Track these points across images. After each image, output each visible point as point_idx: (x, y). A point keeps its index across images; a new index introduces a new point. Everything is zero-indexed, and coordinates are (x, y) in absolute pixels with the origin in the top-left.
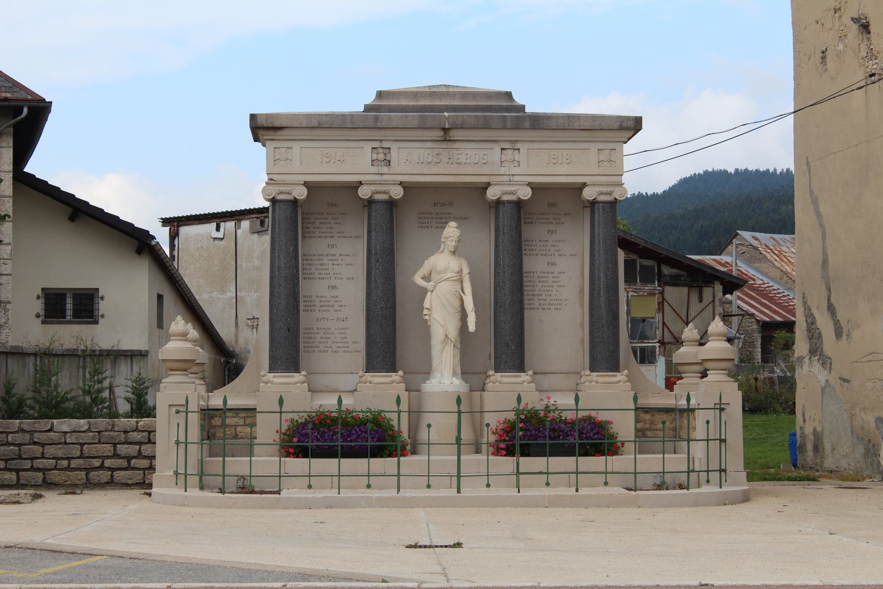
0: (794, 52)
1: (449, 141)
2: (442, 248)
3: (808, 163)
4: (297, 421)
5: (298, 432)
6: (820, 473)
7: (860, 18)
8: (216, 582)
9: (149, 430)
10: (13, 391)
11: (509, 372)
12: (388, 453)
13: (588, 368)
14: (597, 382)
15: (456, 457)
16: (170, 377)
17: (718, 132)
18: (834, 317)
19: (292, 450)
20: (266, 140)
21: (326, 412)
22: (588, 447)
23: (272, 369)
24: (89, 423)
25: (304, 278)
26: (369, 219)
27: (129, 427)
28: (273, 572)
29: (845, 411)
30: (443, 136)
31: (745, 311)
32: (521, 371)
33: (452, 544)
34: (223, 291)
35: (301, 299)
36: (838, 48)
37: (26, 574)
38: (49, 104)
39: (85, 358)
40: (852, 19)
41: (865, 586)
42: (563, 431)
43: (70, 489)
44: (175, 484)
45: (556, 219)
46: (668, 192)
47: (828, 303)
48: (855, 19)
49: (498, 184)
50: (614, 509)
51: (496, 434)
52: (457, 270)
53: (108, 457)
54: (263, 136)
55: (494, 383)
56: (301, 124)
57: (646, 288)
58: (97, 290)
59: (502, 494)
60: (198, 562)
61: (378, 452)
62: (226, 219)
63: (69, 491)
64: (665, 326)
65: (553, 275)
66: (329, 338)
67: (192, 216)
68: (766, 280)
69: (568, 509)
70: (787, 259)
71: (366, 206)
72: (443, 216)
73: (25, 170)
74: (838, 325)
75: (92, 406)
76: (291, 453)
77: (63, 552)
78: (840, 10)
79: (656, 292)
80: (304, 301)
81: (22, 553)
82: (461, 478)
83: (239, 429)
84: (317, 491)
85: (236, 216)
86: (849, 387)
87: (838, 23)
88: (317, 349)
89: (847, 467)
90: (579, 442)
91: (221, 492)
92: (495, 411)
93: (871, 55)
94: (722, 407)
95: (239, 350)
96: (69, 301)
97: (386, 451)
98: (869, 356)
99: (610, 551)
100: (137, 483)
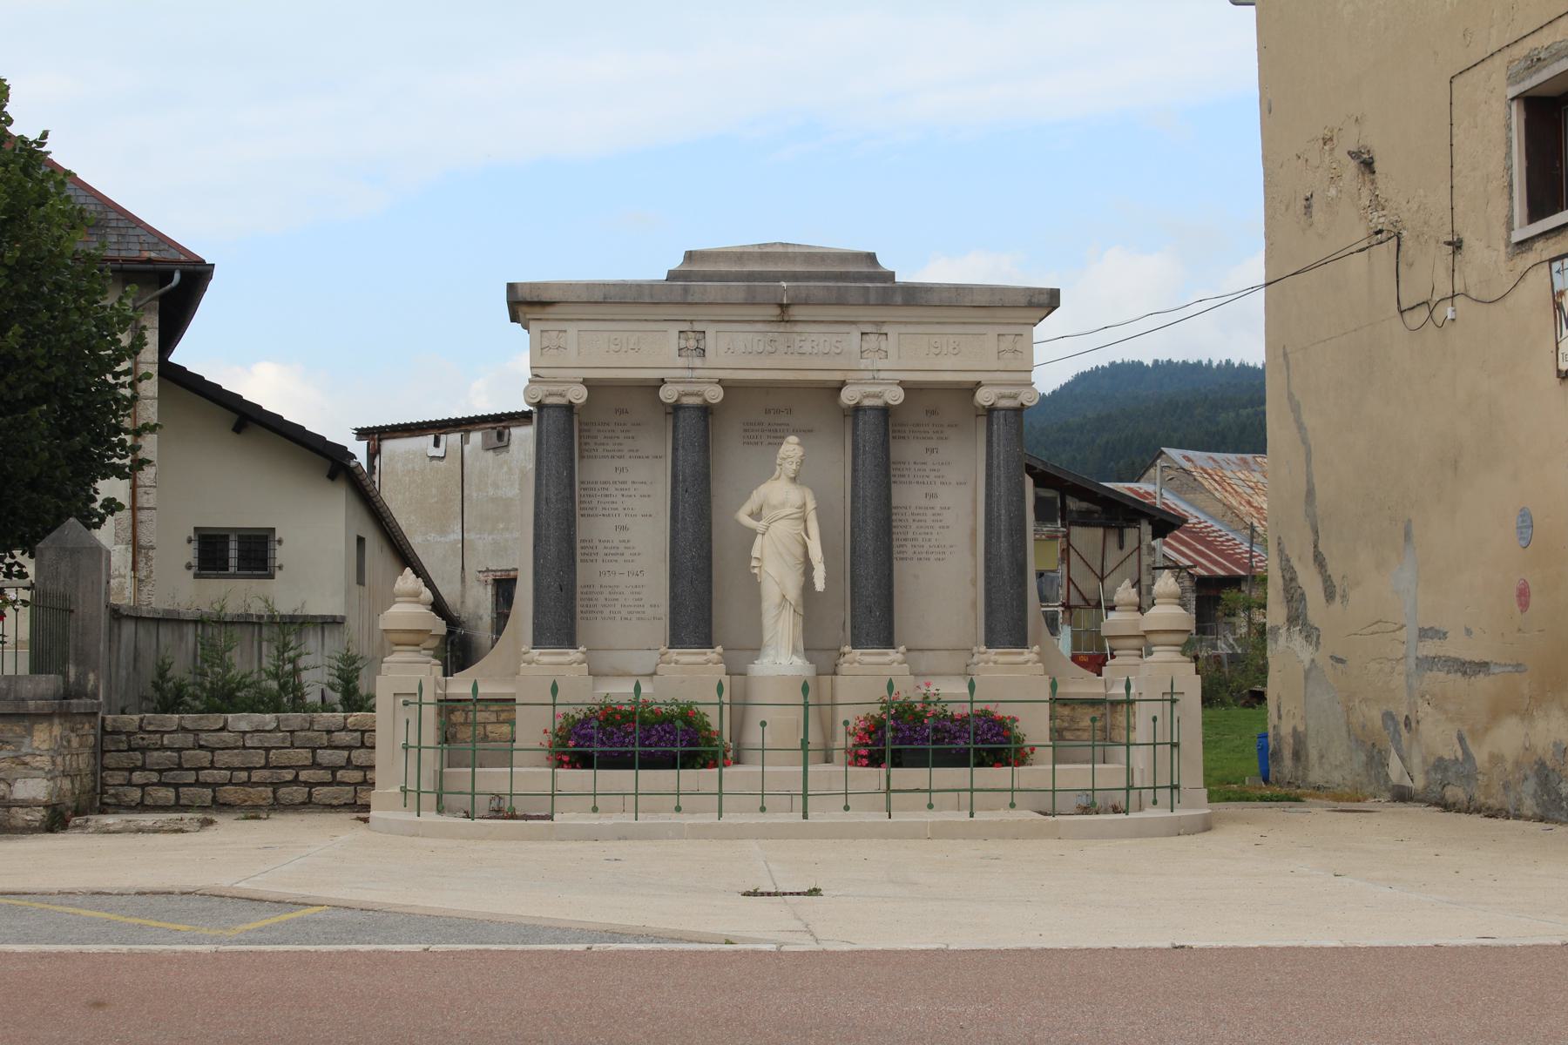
0: (1266, 198)
1: (787, 321)
2: (777, 473)
3: (1285, 355)
4: (573, 716)
7: (1360, 152)
8: (491, 944)
9: (363, 729)
10: (169, 674)
11: (872, 648)
13: (983, 642)
14: (995, 663)
15: (801, 769)
17: (1173, 308)
18: (1323, 570)
19: (565, 758)
21: (614, 704)
22: (985, 754)
23: (537, 643)
24: (278, 718)
25: (582, 515)
26: (674, 432)
28: (568, 929)
30: (780, 315)
31: (1173, 561)
34: (443, 531)
36: (1329, 194)
37: (220, 931)
38: (210, 267)
40: (1349, 153)
41: (1402, 947)
42: (949, 732)
45: (937, 432)
47: (1315, 552)
48: (1354, 153)
49: (858, 383)
52: (799, 503)
53: (305, 767)
54: (525, 314)
56: (579, 297)
57: (1045, 529)
58: (273, 530)
59: (867, 821)
61: (691, 760)
62: (448, 429)
64: (1071, 583)
65: (934, 511)
66: (617, 600)
67: (399, 425)
70: (1233, 489)
72: (778, 428)
73: (170, 359)
75: (280, 695)
76: (565, 762)
78: (1332, 140)
79: (1059, 534)
80: (582, 548)
83: (489, 728)
84: (604, 815)
85: (463, 425)
88: (599, 615)
89: (1341, 782)
90: (975, 746)
93: (1377, 204)
97: (699, 759)
98: (1375, 626)
99: (1030, 899)
100: (345, 804)
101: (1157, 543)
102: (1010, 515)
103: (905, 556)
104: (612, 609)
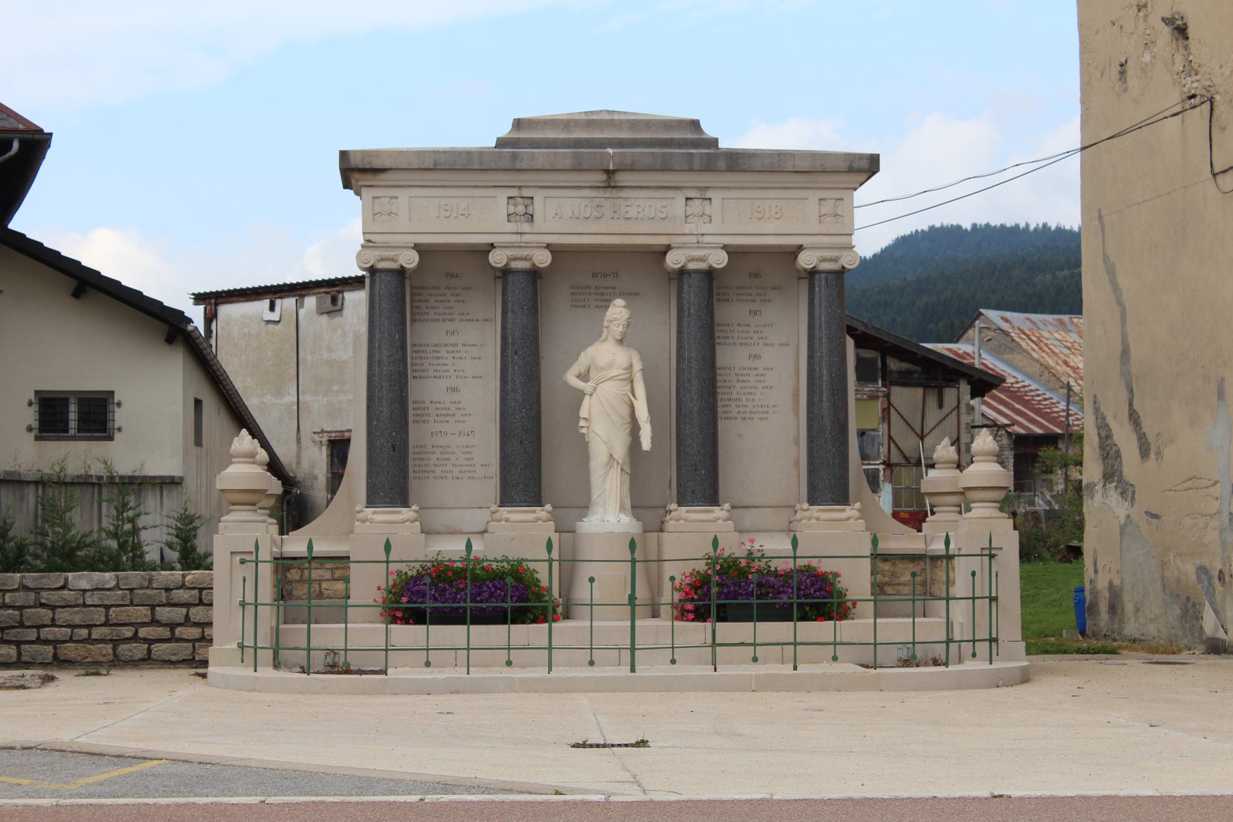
0: (1081, 64)
1: (614, 187)
2: (604, 335)
3: (1100, 218)
4: (406, 573)
5: (408, 589)
6: (1119, 643)
7: (1174, 18)
8: (326, 795)
10: (11, 534)
11: (698, 506)
12: (532, 617)
14: (818, 519)
15: (629, 623)
16: (232, 514)
18: (1138, 428)
20: (361, 186)
21: (446, 561)
23: (371, 502)
24: (117, 577)
25: (414, 377)
27: (172, 582)
29: (1154, 558)
30: (606, 181)
31: (992, 420)
32: (713, 504)
33: (634, 742)
34: (279, 393)
35: (411, 406)
36: (1143, 60)
38: (48, 136)
39: (100, 485)
40: (1163, 19)
42: (773, 587)
43: (91, 669)
44: (240, 662)
45: (761, 295)
46: (880, 255)
47: (1130, 410)
48: (1167, 19)
49: (682, 247)
50: (847, 693)
51: (680, 591)
52: (626, 365)
53: (144, 624)
54: (357, 180)
55: (677, 520)
57: (866, 389)
58: (112, 392)
60: (295, 768)
61: (521, 616)
62: (284, 294)
63: (90, 671)
64: (891, 441)
66: (448, 459)
67: (235, 290)
68: (1020, 378)
69: (783, 693)
71: (500, 277)
72: (605, 291)
74: (1144, 440)
75: (119, 554)
76: (398, 618)
77: (105, 755)
79: (880, 394)
81: (47, 756)
82: (636, 651)
83: (324, 585)
84: (436, 670)
85: (298, 290)
86: (1159, 525)
87: (1143, 24)
88: (431, 475)
91: (305, 673)
92: (683, 560)
93: (1190, 69)
94: (992, 552)
95: (302, 475)
96: (73, 408)
97: (529, 615)
101: (975, 402)
102: (831, 374)
103: (729, 415)
104: (444, 468)
